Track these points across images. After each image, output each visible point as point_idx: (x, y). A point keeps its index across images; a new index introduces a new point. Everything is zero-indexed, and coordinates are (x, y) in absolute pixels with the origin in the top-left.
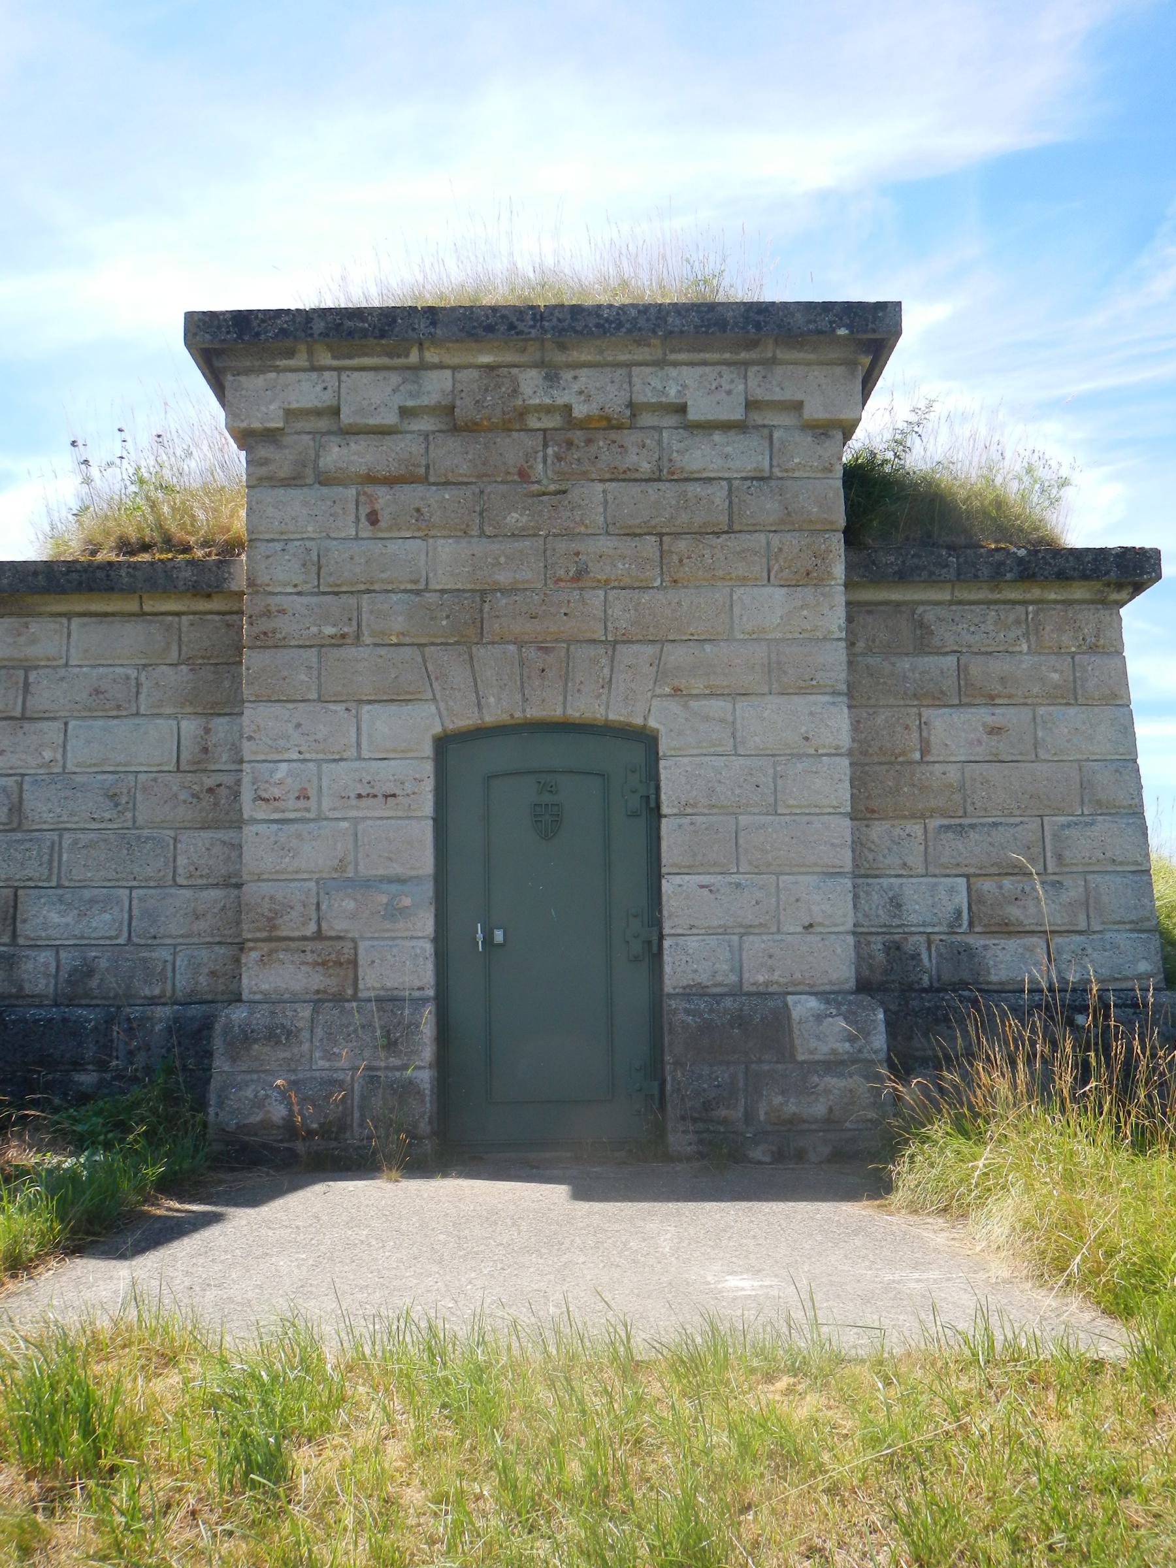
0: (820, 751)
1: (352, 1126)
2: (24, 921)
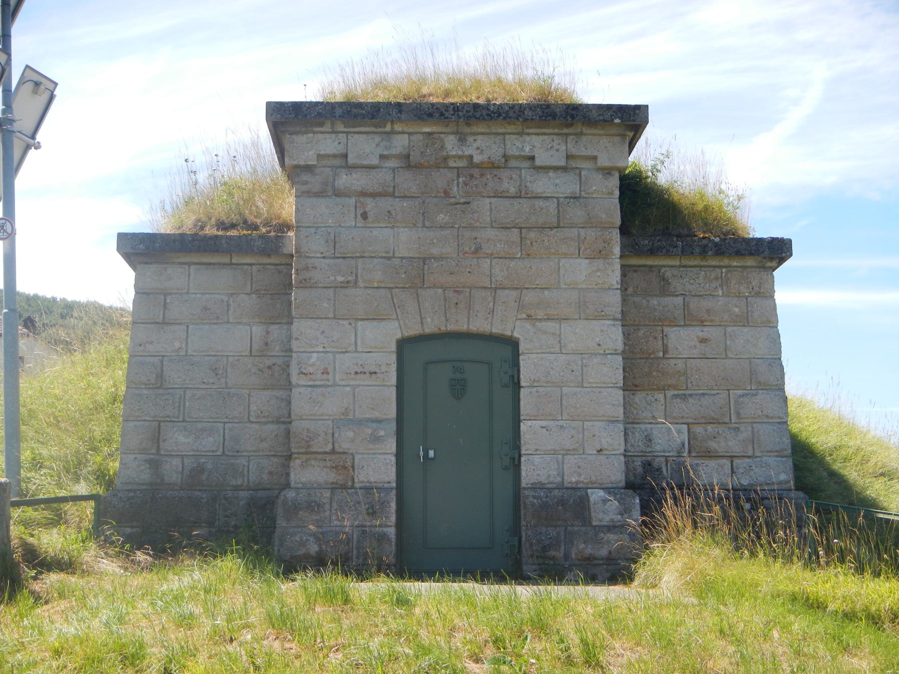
0: (607, 352)
1: (352, 558)
2: (164, 441)
